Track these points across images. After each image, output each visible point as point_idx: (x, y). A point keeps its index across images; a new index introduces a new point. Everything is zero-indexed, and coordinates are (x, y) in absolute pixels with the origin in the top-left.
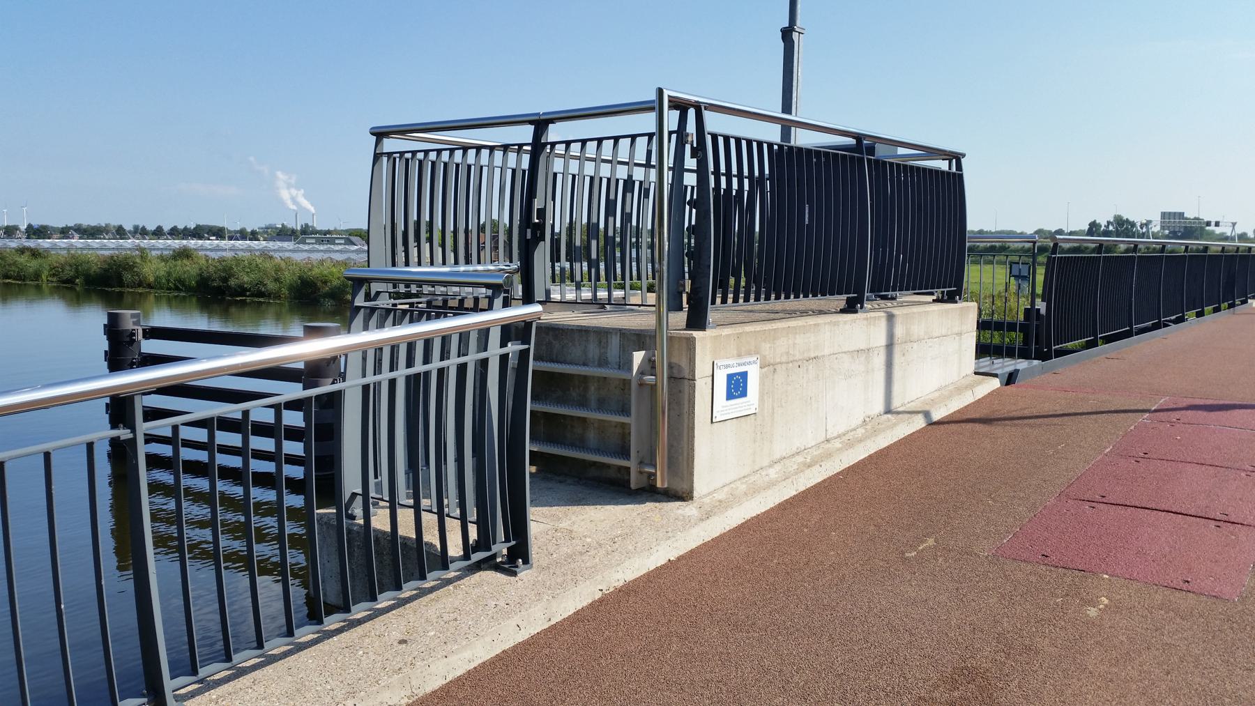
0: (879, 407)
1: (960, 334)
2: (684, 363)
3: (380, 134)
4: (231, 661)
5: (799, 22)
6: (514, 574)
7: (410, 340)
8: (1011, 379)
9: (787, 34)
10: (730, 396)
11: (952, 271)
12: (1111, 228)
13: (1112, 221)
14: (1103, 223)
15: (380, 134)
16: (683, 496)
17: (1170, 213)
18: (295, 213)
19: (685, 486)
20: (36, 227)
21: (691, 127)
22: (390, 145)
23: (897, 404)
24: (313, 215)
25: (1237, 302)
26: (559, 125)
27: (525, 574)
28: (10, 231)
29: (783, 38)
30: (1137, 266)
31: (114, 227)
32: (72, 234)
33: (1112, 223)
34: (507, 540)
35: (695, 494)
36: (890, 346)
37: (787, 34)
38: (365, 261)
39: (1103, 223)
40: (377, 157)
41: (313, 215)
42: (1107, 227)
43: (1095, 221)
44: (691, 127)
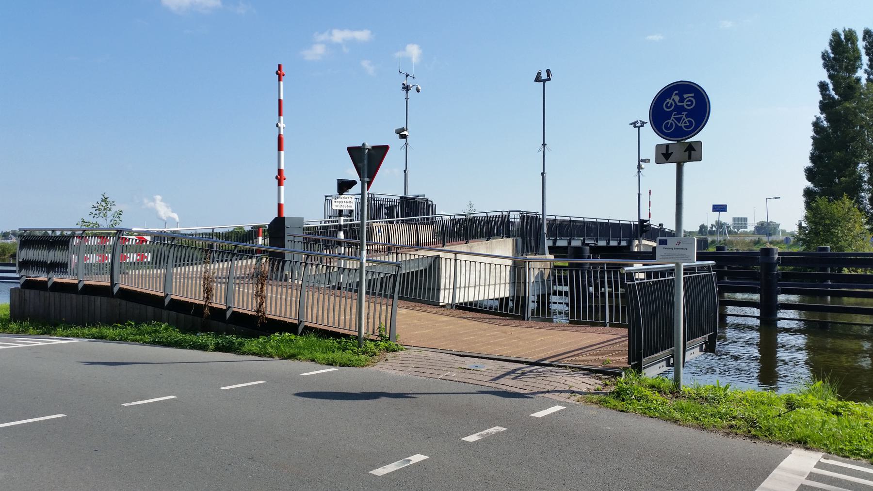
3: (326, 196)
5: (545, 171)
9: (543, 174)
12: (714, 229)
13: (714, 224)
14: (709, 226)
15: (326, 196)
17: (738, 218)
18: (164, 222)
21: (373, 197)
22: (328, 198)
24: (178, 223)
28: (5, 235)
29: (542, 175)
30: (853, 288)
31: (784, 232)
32: (11, 237)
33: (714, 226)
37: (543, 174)
38: (688, 350)
39: (709, 226)
40: (326, 200)
41: (178, 223)
42: (712, 228)
43: (703, 224)
44: (373, 197)
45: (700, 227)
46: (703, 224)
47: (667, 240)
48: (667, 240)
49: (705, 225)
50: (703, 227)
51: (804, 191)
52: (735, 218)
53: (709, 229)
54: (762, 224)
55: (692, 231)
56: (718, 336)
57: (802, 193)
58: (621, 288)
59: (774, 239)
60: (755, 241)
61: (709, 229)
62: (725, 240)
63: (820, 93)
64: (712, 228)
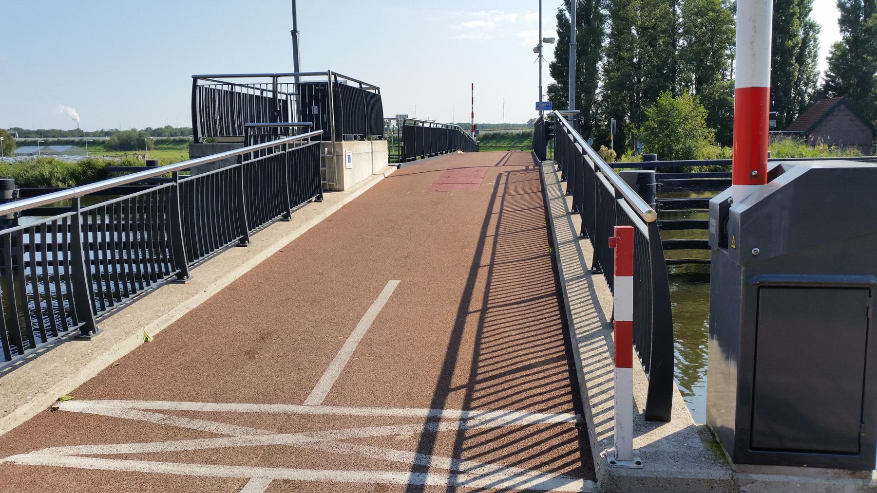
0: (371, 173)
1: (384, 151)
2: (339, 151)
3: (195, 79)
4: (58, 336)
6: (89, 339)
7: (15, 211)
8: (398, 167)
10: (348, 162)
11: (280, 175)
15: (195, 79)
16: (342, 190)
19: (341, 187)
20: (74, 109)
23: (374, 173)
25: (444, 152)
26: (281, 78)
27: (94, 338)
34: (173, 270)
35: (345, 189)
36: (372, 152)
54: (169, 126)
63: (160, 127)
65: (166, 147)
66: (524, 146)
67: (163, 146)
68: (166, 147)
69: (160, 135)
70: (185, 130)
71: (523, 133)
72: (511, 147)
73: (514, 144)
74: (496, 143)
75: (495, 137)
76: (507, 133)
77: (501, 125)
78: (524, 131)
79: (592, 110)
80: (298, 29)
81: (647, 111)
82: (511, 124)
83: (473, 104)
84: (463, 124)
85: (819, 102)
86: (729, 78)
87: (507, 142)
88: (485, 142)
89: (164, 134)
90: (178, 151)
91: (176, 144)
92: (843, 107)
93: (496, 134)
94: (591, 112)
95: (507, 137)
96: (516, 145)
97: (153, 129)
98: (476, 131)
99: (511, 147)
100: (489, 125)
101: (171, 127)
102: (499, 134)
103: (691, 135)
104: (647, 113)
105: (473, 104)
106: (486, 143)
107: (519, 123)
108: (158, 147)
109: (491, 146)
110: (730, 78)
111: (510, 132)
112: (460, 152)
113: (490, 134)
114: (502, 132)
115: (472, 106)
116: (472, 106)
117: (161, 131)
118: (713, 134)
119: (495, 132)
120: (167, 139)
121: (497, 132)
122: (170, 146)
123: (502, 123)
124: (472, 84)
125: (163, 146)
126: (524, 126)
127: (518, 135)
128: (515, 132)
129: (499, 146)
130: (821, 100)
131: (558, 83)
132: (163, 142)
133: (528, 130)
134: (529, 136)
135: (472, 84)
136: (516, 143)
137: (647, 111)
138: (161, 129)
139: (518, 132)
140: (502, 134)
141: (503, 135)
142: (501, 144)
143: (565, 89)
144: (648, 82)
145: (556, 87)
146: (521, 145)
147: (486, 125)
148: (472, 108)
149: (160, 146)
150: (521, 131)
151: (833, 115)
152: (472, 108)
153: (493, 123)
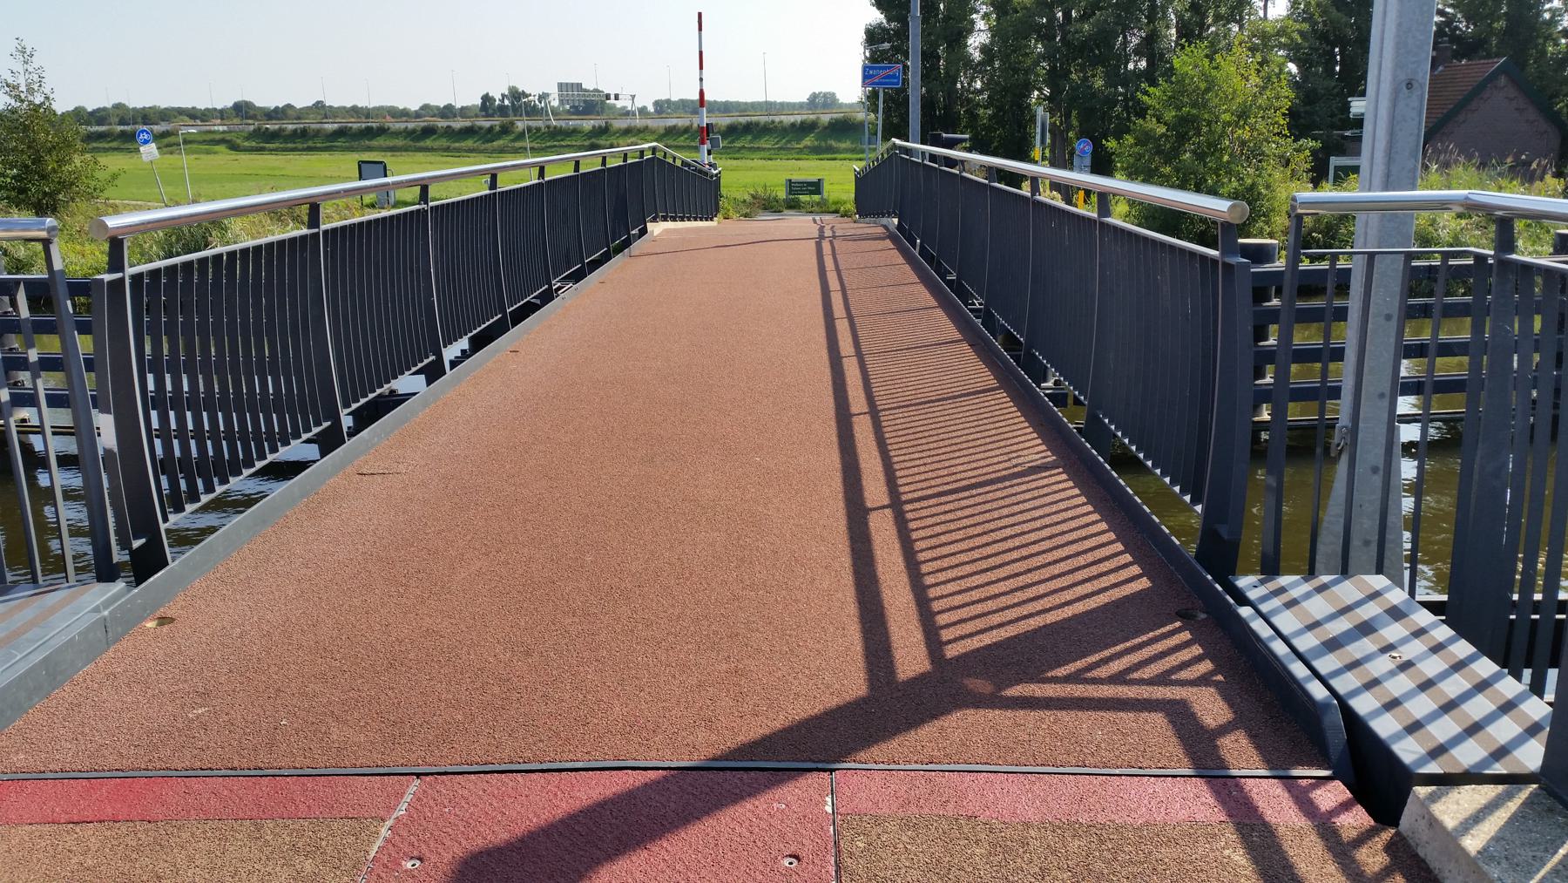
12: (507, 102)
14: (498, 97)
39: (498, 97)
42: (503, 101)
43: (488, 94)
45: (482, 98)
46: (488, 94)
47: (1335, 167)
48: (1335, 167)
49: (490, 95)
50: (486, 99)
51: (76, 108)
52: (561, 84)
53: (497, 102)
54: (120, 104)
55: (465, 105)
56: (168, 531)
57: (861, 36)
58: (170, 546)
59: (632, 125)
60: (600, 127)
61: (497, 102)
62: (548, 127)
63: (102, 106)
64: (503, 101)
65: (106, 146)
66: (805, 147)
67: (101, 145)
68: (106, 146)
69: (101, 122)
70: (152, 111)
71: (802, 123)
72: (780, 149)
73: (786, 144)
74: (751, 142)
75: (749, 129)
76: (773, 122)
77: (759, 104)
78: (805, 117)
79: (962, 83)
80: (703, 50)
81: (1146, 93)
82: (778, 101)
83: (701, 68)
84: (690, 100)
85: (1441, 68)
86: (1261, 13)
87: (772, 139)
88: (730, 139)
89: (108, 121)
90: (130, 155)
91: (125, 142)
92: (1503, 80)
93: (751, 123)
94: (959, 86)
95: (772, 129)
96: (789, 146)
97: (89, 110)
98: (711, 140)
99: (780, 149)
100: (738, 104)
101: (124, 105)
102: (757, 124)
103: (1254, 154)
104: (1145, 98)
105: (701, 68)
106: (732, 142)
107: (792, 101)
108: (90, 146)
109: (743, 147)
110: (1262, 16)
111: (777, 119)
112: (656, 228)
113: (741, 124)
114: (763, 119)
115: (701, 73)
116: (701, 73)
117: (104, 113)
118: (1308, 153)
119: (748, 119)
120: (109, 130)
121: (754, 119)
122: (114, 144)
123: (761, 99)
124: (700, 15)
125: (101, 145)
126: (801, 105)
127: (793, 125)
128: (788, 120)
129: (758, 148)
130: (1446, 65)
131: (889, 20)
132: (100, 136)
133: (811, 117)
134: (814, 129)
135: (700, 15)
136: (789, 142)
137: (1146, 93)
138: (105, 109)
139: (792, 119)
140: (762, 124)
141: (765, 125)
142: (763, 143)
143: (902, 34)
144: (1099, 20)
145: (884, 30)
146: (798, 146)
147: (731, 103)
148: (701, 80)
149: (95, 145)
150: (799, 119)
151: (1482, 98)
152: (701, 80)
153: (744, 101)
